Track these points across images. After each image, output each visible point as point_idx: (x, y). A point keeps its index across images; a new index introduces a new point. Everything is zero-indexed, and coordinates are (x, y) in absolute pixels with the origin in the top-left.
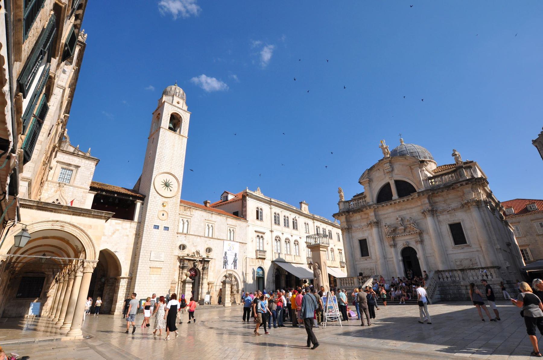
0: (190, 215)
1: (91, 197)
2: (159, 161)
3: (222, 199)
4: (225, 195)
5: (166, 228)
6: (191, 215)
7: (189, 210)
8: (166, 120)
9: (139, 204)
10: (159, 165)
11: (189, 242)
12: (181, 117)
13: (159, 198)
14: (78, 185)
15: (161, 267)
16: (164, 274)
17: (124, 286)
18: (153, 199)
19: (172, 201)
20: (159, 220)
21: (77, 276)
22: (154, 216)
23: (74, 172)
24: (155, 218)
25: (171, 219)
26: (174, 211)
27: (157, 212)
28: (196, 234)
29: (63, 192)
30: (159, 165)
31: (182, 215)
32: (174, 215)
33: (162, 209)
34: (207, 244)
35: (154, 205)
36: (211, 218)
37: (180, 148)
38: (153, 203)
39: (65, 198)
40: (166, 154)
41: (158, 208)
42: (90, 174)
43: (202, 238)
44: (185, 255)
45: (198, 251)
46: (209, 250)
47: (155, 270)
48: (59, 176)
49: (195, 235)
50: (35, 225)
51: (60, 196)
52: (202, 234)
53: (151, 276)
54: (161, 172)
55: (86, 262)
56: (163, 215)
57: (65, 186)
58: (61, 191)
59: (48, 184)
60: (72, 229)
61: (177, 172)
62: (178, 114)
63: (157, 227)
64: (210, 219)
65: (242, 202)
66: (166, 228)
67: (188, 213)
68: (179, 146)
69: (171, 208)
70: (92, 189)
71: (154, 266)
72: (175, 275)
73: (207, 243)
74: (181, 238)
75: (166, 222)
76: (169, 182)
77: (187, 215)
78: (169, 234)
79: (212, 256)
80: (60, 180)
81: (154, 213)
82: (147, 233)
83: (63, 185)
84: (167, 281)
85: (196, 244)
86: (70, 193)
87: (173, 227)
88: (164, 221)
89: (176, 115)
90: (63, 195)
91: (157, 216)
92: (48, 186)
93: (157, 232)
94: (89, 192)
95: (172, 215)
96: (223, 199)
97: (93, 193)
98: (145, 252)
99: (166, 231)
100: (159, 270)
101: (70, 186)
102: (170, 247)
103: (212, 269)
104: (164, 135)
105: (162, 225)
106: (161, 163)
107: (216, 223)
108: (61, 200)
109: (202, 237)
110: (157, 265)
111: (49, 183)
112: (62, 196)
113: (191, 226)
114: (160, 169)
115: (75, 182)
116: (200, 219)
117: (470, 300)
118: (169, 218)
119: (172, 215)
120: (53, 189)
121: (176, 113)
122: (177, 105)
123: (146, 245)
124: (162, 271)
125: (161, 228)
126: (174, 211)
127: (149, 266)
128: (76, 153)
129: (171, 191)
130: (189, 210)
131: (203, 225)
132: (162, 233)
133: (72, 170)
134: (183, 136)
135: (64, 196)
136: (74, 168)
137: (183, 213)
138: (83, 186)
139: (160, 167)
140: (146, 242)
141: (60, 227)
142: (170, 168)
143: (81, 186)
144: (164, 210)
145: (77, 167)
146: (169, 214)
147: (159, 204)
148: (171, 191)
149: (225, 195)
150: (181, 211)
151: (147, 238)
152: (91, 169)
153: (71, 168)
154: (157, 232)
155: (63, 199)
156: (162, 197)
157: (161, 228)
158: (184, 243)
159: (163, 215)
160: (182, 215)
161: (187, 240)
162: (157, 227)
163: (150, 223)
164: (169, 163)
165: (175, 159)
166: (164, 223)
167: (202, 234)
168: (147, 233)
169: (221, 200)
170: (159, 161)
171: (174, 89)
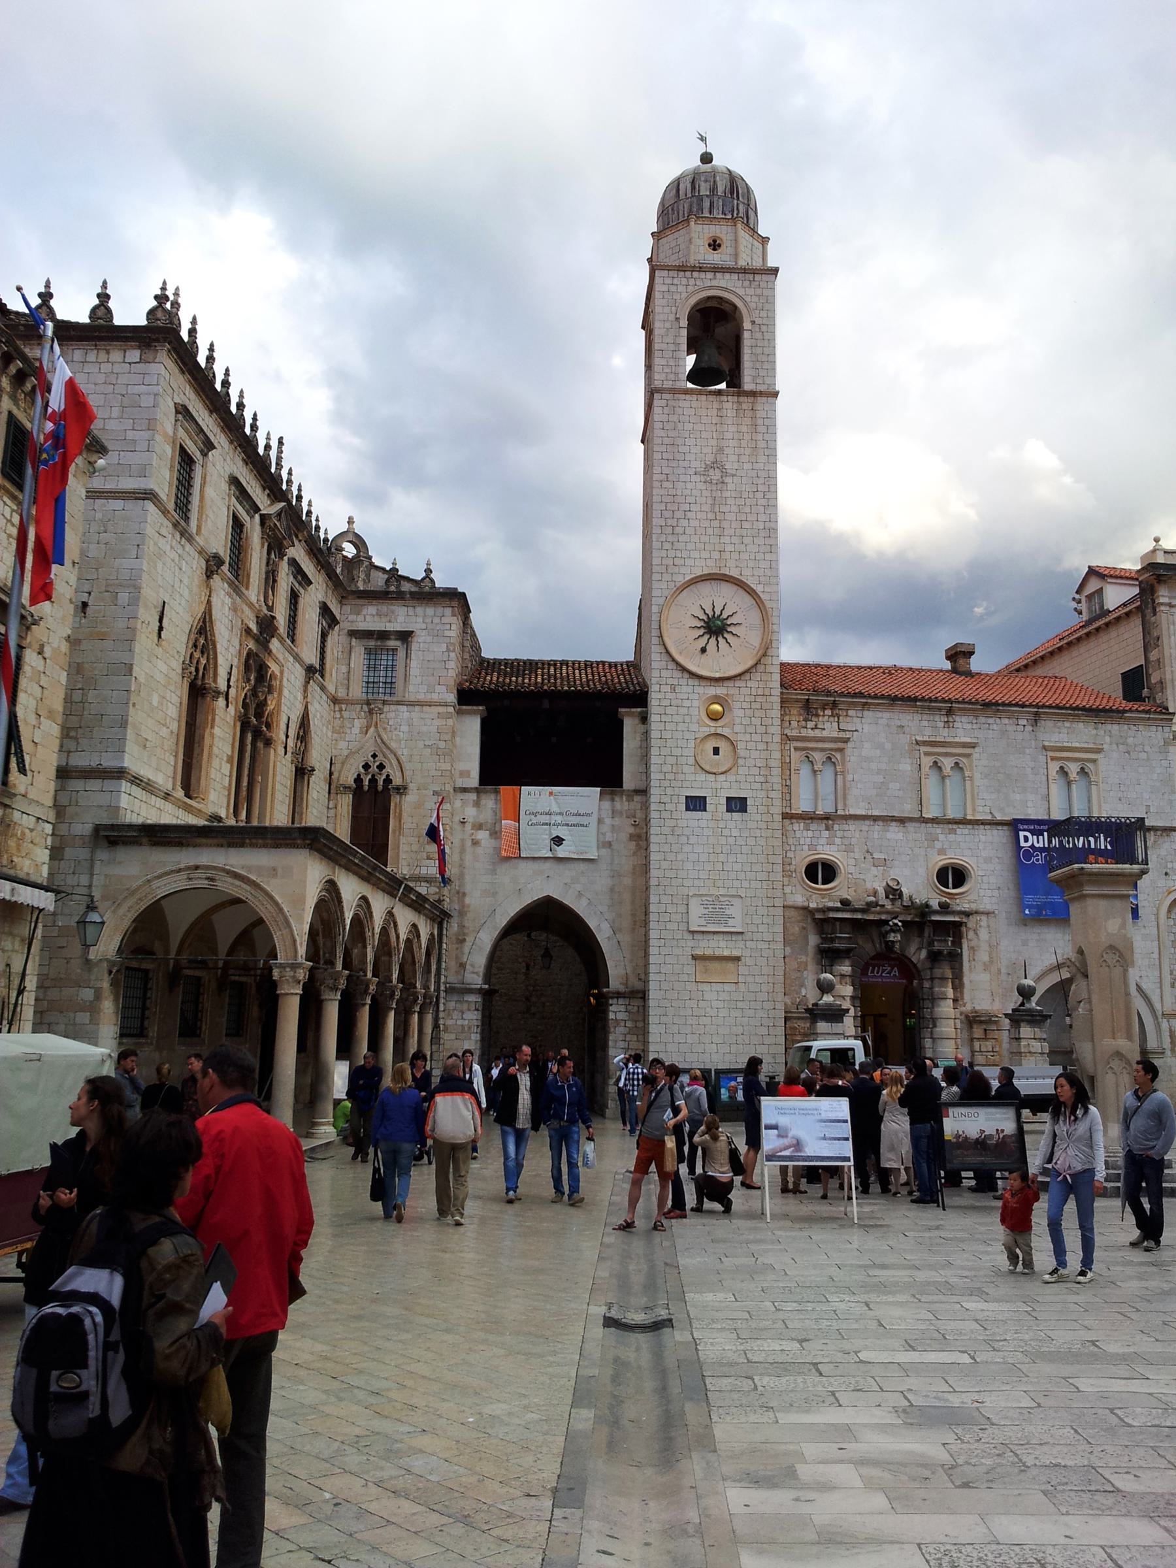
0: (835, 734)
1: (470, 729)
2: (670, 538)
3: (1083, 606)
4: (1093, 585)
5: (737, 805)
6: (842, 735)
7: (828, 712)
8: (672, 347)
9: (630, 725)
10: (671, 553)
11: (849, 849)
12: (735, 307)
13: (690, 689)
14: (421, 697)
15: (736, 953)
16: (750, 979)
17: (623, 1024)
18: (669, 696)
19: (747, 691)
20: (702, 777)
21: (322, 1001)
22: (683, 760)
23: (401, 654)
24: (686, 769)
25: (751, 762)
26: (761, 729)
27: (692, 744)
28: (876, 813)
29: (385, 729)
30: (671, 553)
31: (797, 739)
32: (761, 746)
33: (706, 731)
34: (941, 852)
35: (676, 718)
36: (945, 732)
37: (748, 451)
38: (669, 710)
39: (393, 745)
40: (689, 500)
41: (694, 727)
42: (448, 650)
43: (911, 826)
44: (831, 904)
45: (893, 884)
46: (953, 876)
47: (715, 965)
48: (365, 679)
49: (875, 819)
50: (156, 884)
51: (379, 740)
52: (908, 807)
53: (702, 987)
54: (681, 580)
55: (277, 967)
56: (716, 751)
57: (386, 708)
58: (376, 726)
59: (341, 710)
60: (232, 884)
61: (751, 564)
62: (721, 298)
63: (696, 804)
64: (944, 735)
65: (1143, 617)
66: (737, 805)
67: (827, 725)
68: (744, 443)
69: (746, 721)
70: (466, 697)
71: (709, 952)
72: (802, 985)
73: (938, 845)
74: (810, 834)
75: (731, 777)
76: (724, 616)
77: (825, 734)
78: (751, 825)
79: (975, 901)
80: (370, 690)
81: (678, 752)
82: (666, 830)
83: (381, 706)
84: (766, 1005)
85: (882, 856)
86: (405, 728)
87: (763, 794)
88: (722, 778)
89: (714, 304)
90: (385, 737)
91: (691, 761)
92: (342, 717)
93: (703, 824)
94: (459, 713)
95: (751, 745)
96: (1084, 611)
97: (474, 713)
98: (665, 899)
99: (736, 816)
100: (731, 966)
101: (399, 703)
102: (763, 876)
103: (983, 956)
104: (674, 418)
105: (717, 791)
106: (677, 545)
107: (977, 750)
108: (385, 756)
109: (911, 819)
110: (724, 947)
111: (344, 707)
112: (384, 743)
113: (850, 777)
114: (676, 570)
115: (411, 688)
116: (888, 746)
117: (1041, 1174)
118: (741, 762)
119: (751, 745)
120: (357, 723)
121: (709, 298)
122: (715, 258)
123: (669, 874)
124: (743, 970)
125: (717, 805)
126: (761, 729)
127: (689, 951)
128: (393, 588)
129: (703, 650)
130: (828, 712)
131: (906, 766)
132: (722, 824)
133: (394, 650)
134: (753, 394)
135: (388, 742)
136: (398, 643)
137: (804, 732)
138: (435, 697)
139: (677, 561)
140: (665, 865)
141: (206, 882)
142: (716, 555)
143: (429, 697)
144: (719, 731)
145: (405, 636)
146: (740, 745)
147: (695, 712)
148: (703, 650)
149: (1093, 585)
150: (794, 724)
151: (666, 848)
152: (447, 633)
153: (392, 643)
154: (703, 824)
155: (387, 752)
156: (703, 683)
157: (717, 805)
158: (829, 852)
159: (716, 751)
160: (797, 739)
161: (838, 841)
162: (696, 804)
163: (669, 791)
164: (710, 531)
165: (734, 508)
166: (725, 785)
167: (908, 809)
168: (666, 830)
169: (1080, 613)
170: (670, 538)
171: (689, 186)
